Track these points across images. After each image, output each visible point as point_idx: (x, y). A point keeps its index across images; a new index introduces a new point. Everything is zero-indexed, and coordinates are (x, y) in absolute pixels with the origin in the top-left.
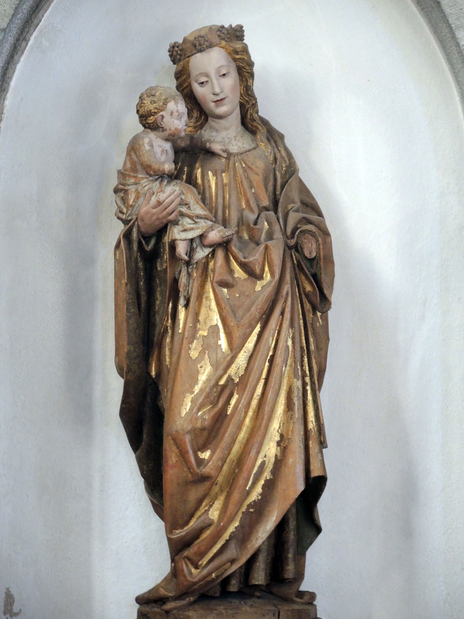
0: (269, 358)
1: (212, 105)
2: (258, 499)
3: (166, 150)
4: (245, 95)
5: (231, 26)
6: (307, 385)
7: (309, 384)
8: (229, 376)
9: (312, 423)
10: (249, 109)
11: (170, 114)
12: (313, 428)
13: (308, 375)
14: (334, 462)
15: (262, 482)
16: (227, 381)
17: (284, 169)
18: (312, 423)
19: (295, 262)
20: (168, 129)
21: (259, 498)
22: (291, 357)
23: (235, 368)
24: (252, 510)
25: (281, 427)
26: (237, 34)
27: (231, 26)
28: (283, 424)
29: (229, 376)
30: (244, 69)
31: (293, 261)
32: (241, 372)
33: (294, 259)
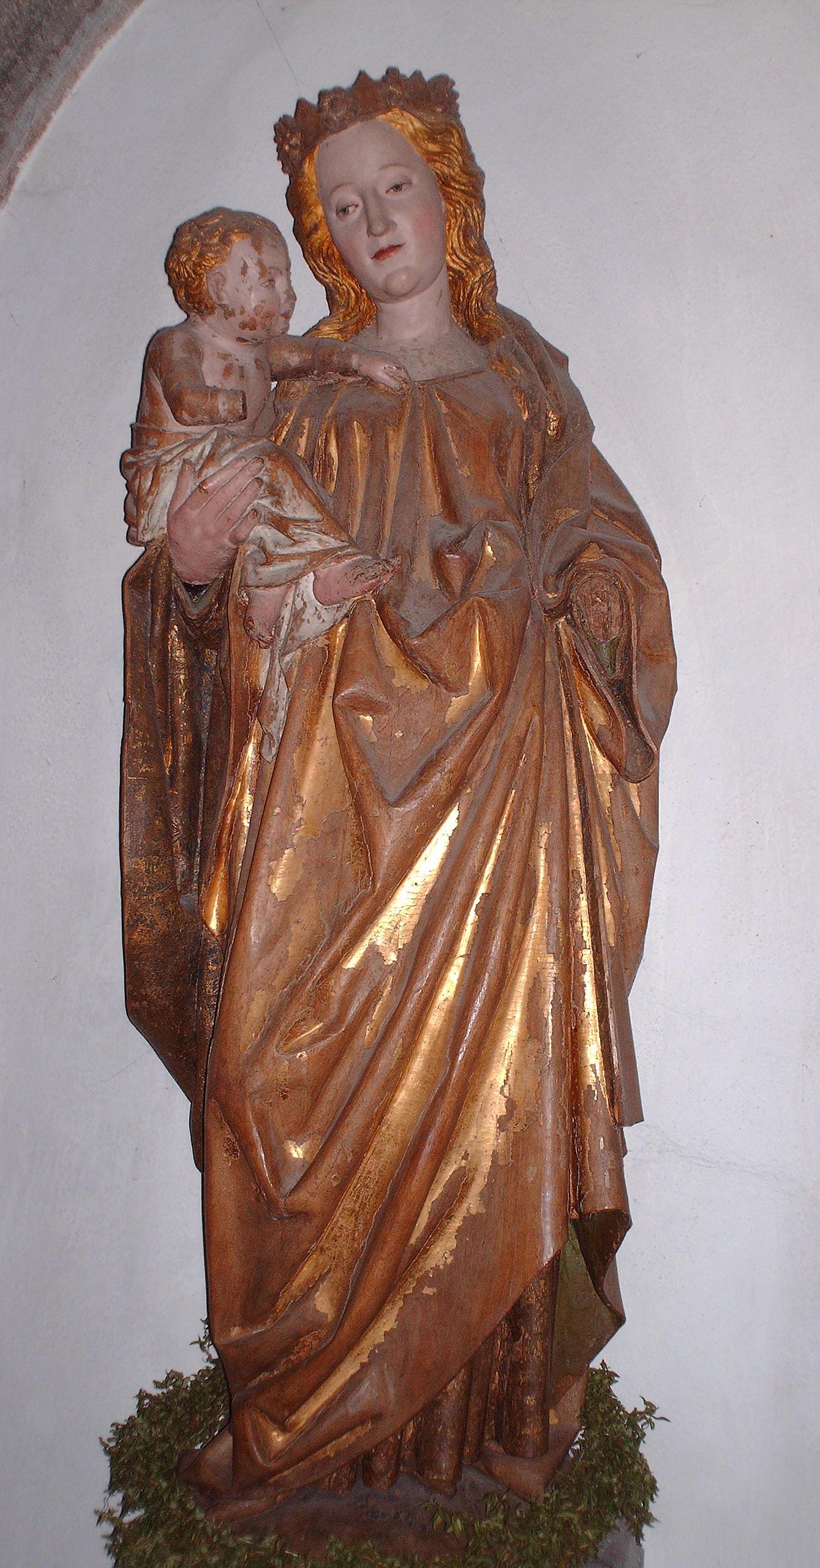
0: (477, 901)
1: (368, 261)
2: (445, 1264)
3: (242, 368)
4: (462, 251)
5: (417, 75)
6: (584, 972)
7: (588, 967)
8: (373, 947)
9: (595, 1071)
10: (477, 285)
11: (239, 271)
12: (597, 1084)
13: (589, 944)
14: (654, 1172)
15: (456, 1223)
16: (365, 959)
17: (553, 424)
18: (595, 1071)
19: (566, 652)
20: (237, 312)
21: (449, 1261)
22: (542, 899)
23: (387, 926)
24: (428, 1291)
25: (510, 1081)
26: (433, 98)
27: (417, 75)
28: (516, 1072)
29: (373, 947)
30: (459, 188)
31: (560, 647)
32: (404, 939)
33: (564, 644)
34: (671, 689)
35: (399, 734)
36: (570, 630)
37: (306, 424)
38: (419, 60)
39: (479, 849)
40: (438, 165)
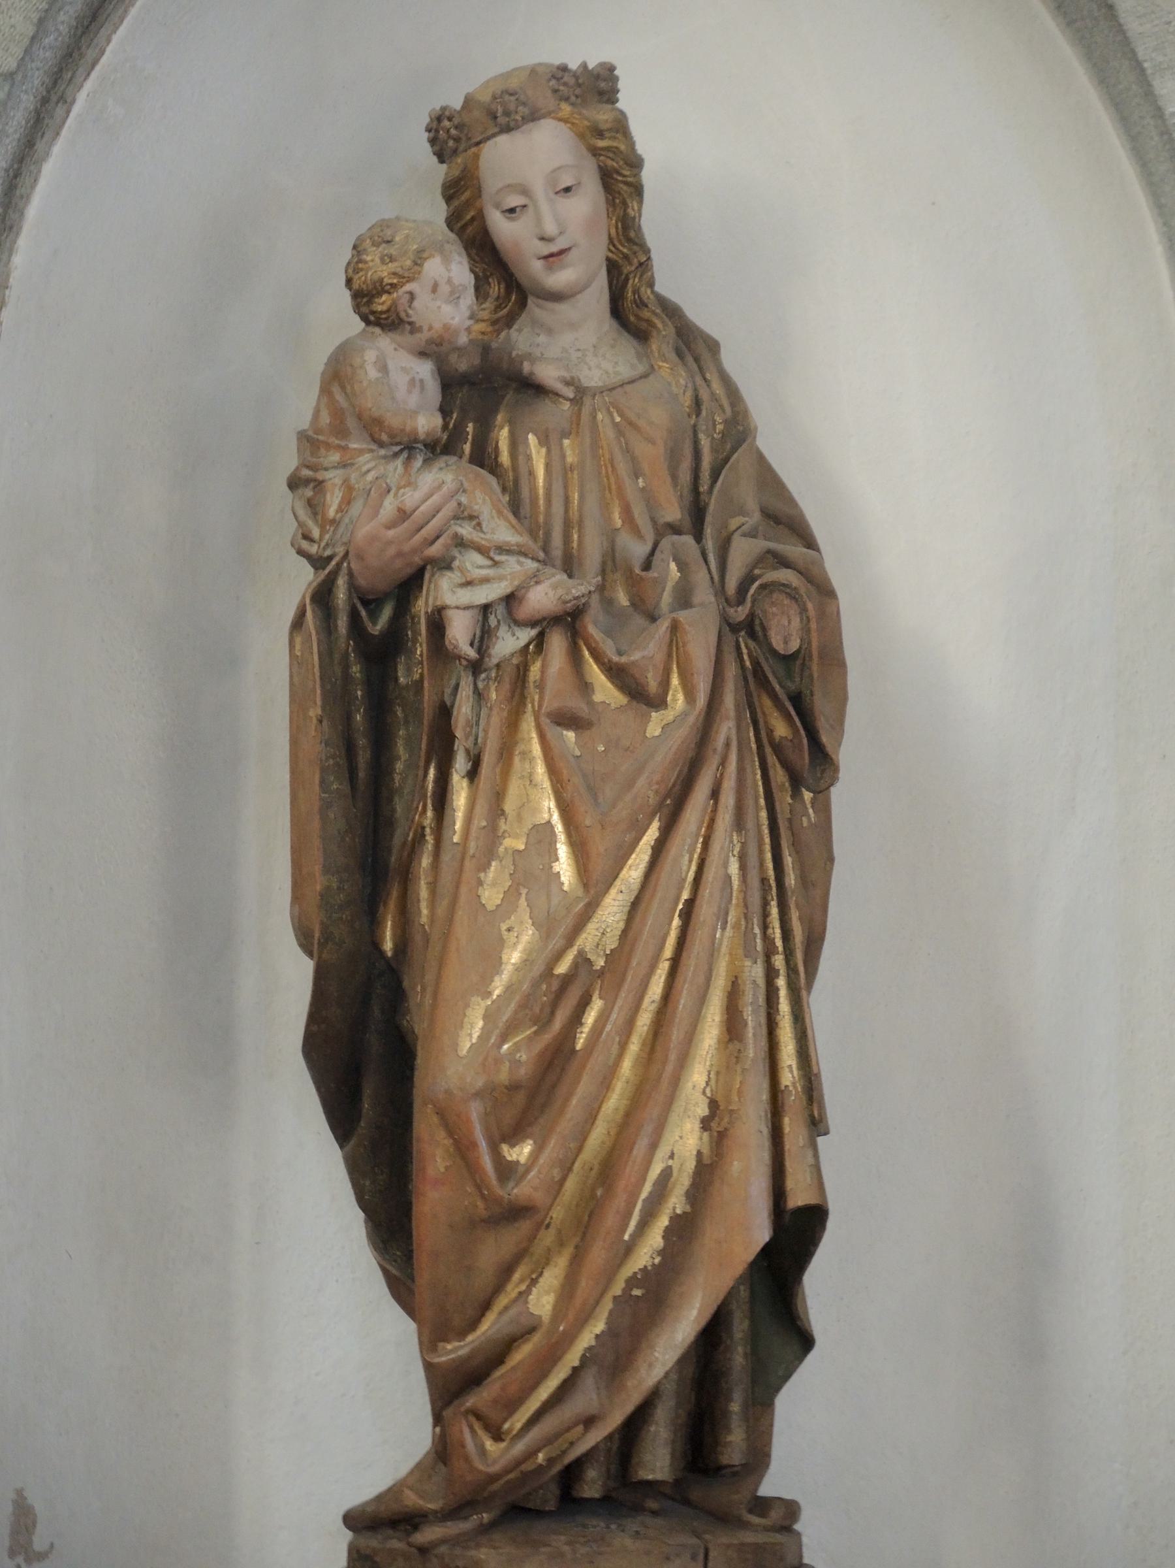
0: (680, 906)
1: (537, 266)
2: (654, 1264)
3: (421, 381)
4: (620, 241)
5: (584, 66)
6: (778, 976)
9: (791, 1072)
12: (794, 1084)
13: (781, 949)
14: (845, 1171)
15: (663, 1221)
16: (575, 965)
18: (791, 1072)
19: (748, 663)
20: (425, 328)
22: (737, 905)
24: (637, 1292)
25: (713, 1083)
27: (584, 66)
28: (718, 1073)
32: (611, 943)
33: (746, 657)
34: (843, 700)
35: (601, 748)
36: (752, 644)
37: (470, 428)
38: (580, 52)
39: (687, 858)
40: (602, 158)
